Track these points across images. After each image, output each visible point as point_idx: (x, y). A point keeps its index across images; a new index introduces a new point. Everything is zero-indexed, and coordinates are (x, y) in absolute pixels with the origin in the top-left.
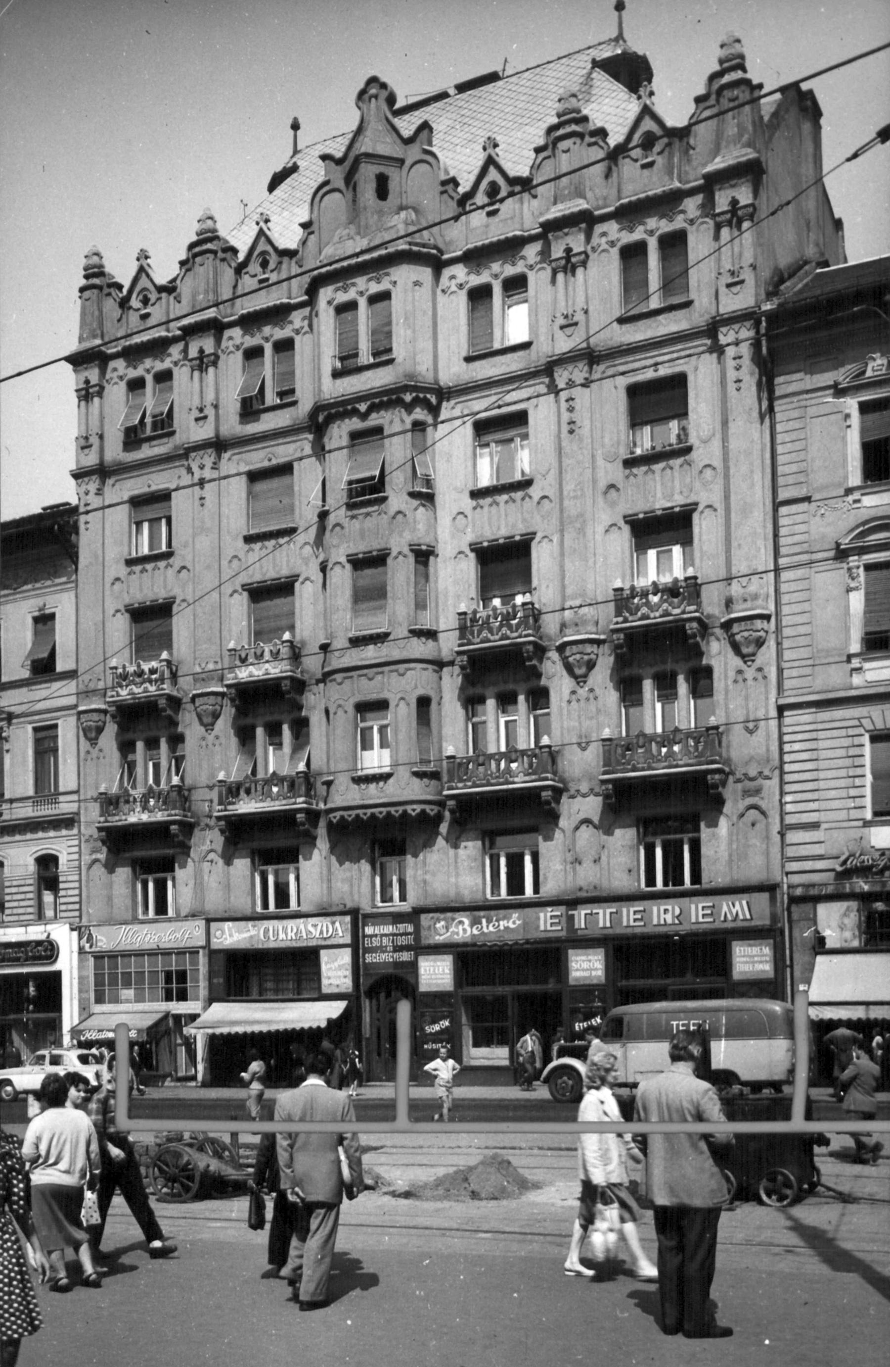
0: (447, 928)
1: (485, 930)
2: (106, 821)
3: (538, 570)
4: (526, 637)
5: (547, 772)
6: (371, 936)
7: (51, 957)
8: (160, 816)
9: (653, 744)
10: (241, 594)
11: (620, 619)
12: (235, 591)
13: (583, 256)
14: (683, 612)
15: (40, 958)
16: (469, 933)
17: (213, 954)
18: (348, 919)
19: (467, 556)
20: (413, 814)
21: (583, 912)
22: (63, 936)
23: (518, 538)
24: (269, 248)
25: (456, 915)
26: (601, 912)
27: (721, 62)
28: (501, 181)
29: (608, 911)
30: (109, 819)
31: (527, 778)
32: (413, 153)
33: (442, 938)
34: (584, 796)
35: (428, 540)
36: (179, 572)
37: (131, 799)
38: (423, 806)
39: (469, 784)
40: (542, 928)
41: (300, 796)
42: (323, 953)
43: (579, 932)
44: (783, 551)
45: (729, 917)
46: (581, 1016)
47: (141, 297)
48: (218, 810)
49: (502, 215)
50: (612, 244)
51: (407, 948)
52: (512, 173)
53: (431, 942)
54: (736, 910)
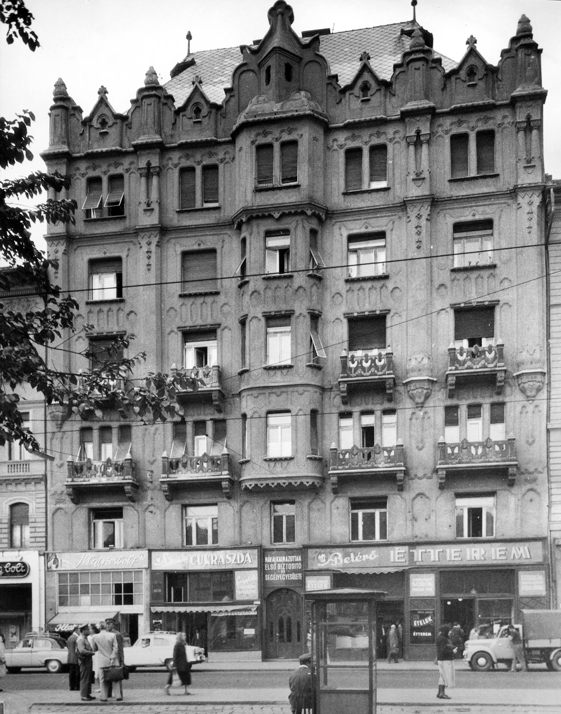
0: (327, 559)
1: (353, 560)
2: (73, 481)
3: (391, 334)
4: (388, 375)
5: (401, 462)
6: (270, 563)
7: (25, 573)
8: (116, 479)
9: (472, 447)
10: (176, 333)
11: (454, 368)
12: (172, 331)
13: (158, 169)
14: (496, 366)
15: (15, 574)
16: (341, 562)
17: (154, 574)
18: (256, 551)
19: (341, 321)
20: (308, 485)
21: (420, 551)
22: (32, 558)
23: (378, 312)
24: (202, 102)
25: (333, 550)
26: (432, 551)
27: (147, 83)
28: (372, 83)
29: (437, 551)
30: (75, 479)
31: (387, 465)
32: (308, 55)
33: (322, 565)
34: (420, 478)
35: (318, 307)
36: (128, 314)
37: (93, 467)
38: (256, 482)
39: (347, 467)
40: (392, 560)
41: (225, 470)
42: (236, 573)
43: (418, 564)
44: (552, 335)
45: (517, 557)
46: (418, 617)
47: (100, 120)
48: (163, 477)
49: (371, 104)
50: (341, 146)
51: (296, 571)
52: (212, 101)
53: (315, 568)
54: (519, 553)
